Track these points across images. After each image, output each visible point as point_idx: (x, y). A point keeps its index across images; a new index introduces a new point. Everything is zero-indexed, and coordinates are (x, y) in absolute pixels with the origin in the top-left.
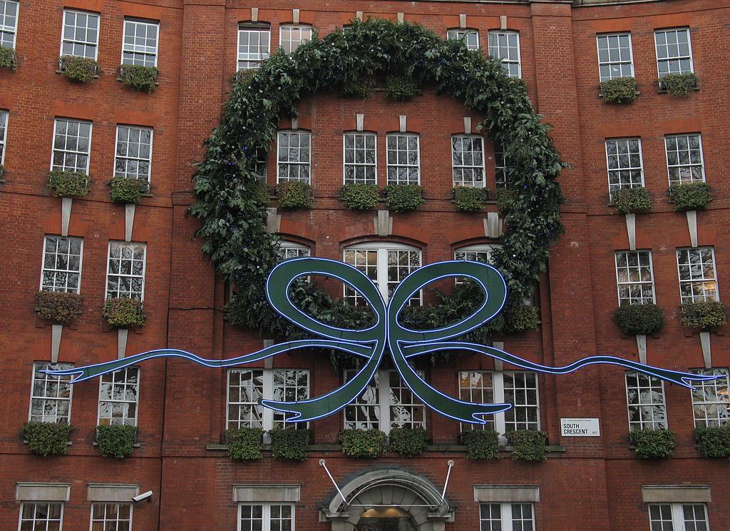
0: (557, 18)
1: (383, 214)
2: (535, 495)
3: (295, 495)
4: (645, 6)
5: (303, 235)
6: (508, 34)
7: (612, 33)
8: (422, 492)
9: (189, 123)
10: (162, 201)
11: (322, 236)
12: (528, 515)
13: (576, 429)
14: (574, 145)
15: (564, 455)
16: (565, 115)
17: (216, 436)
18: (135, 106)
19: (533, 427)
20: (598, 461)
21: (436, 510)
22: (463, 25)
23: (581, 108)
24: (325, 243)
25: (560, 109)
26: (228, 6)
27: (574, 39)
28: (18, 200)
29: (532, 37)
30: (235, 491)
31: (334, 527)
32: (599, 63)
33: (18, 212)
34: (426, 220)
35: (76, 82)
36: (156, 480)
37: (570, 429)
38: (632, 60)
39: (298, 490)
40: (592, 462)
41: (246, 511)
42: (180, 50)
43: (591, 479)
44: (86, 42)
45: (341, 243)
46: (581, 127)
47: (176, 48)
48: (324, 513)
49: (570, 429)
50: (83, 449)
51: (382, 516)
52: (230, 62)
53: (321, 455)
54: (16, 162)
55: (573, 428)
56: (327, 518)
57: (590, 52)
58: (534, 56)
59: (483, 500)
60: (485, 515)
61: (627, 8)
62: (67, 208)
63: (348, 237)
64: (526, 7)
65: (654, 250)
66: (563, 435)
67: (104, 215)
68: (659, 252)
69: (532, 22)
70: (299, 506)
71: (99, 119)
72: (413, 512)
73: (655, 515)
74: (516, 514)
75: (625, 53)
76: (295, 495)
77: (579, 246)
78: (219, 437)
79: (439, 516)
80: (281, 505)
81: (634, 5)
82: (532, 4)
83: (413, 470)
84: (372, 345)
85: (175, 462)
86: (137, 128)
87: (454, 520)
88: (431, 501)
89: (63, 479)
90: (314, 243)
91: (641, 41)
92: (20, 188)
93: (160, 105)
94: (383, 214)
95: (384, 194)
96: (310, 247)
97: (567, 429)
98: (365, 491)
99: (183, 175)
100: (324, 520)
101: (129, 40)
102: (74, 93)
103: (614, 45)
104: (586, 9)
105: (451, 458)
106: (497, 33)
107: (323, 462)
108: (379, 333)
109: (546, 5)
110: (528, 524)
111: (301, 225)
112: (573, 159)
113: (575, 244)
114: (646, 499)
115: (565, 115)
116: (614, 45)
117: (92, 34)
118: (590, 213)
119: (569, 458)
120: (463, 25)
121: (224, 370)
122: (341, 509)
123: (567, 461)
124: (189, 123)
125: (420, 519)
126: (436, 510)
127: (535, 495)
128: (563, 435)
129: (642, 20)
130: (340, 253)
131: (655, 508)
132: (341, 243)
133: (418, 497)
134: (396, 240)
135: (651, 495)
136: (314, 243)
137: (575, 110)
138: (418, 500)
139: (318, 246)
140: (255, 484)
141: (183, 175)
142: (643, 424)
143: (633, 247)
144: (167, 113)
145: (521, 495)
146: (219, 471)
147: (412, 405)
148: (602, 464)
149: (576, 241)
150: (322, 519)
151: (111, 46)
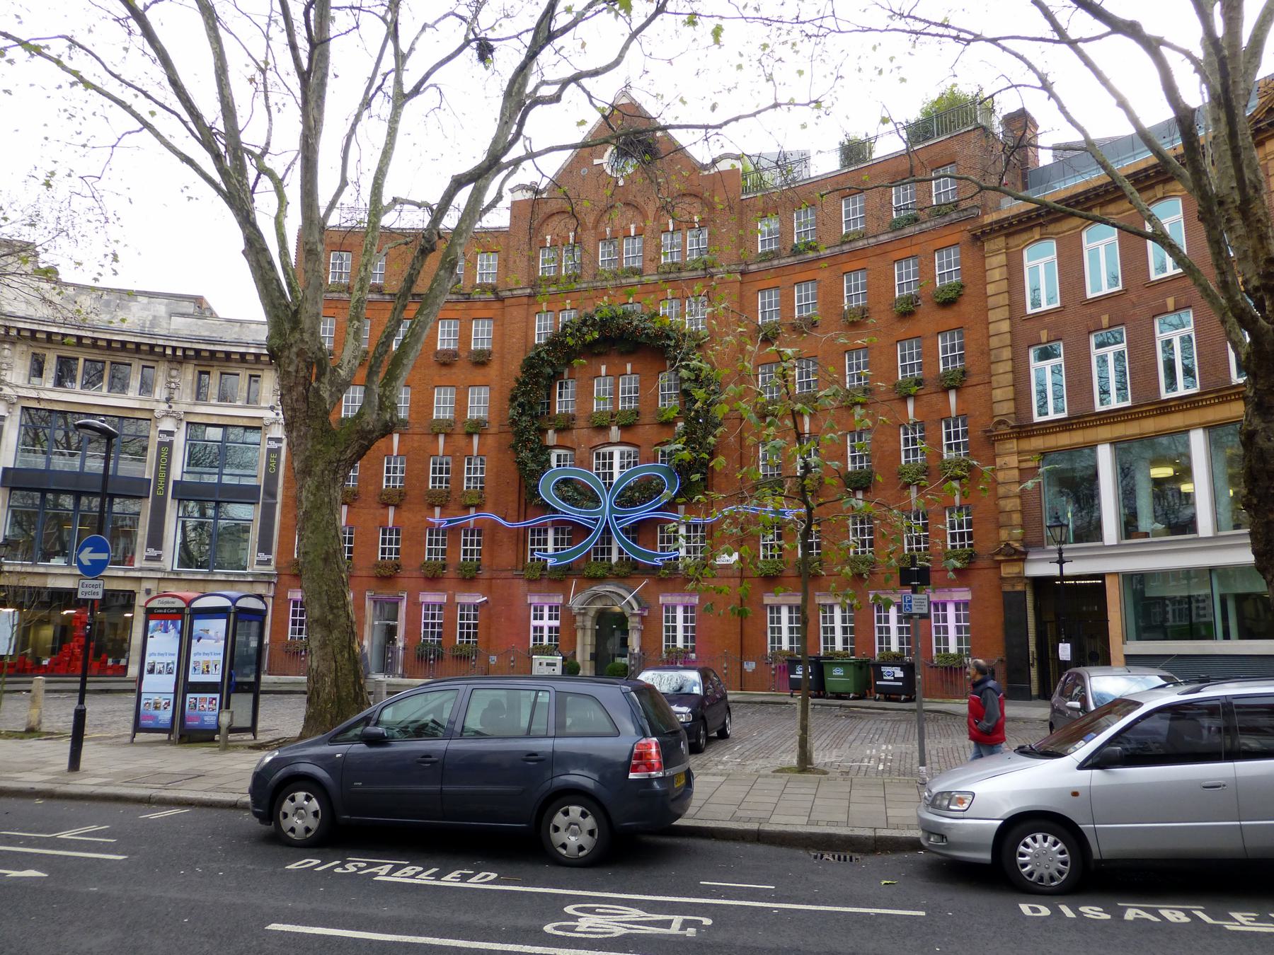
1: (614, 429)
5: (569, 445)
10: (493, 430)
11: (579, 445)
17: (520, 567)
18: (479, 374)
22: (670, 297)
28: (416, 437)
33: (416, 445)
34: (640, 430)
35: (444, 364)
36: (489, 591)
40: (732, 580)
42: (503, 335)
47: (500, 336)
50: (452, 575)
54: (414, 416)
62: (441, 439)
67: (460, 441)
73: (772, 612)
83: (1089, 209)
84: (597, 520)
89: (443, 591)
92: (417, 430)
93: (493, 371)
94: (614, 429)
95: (613, 416)
102: (444, 371)
108: (603, 512)
111: (569, 439)
114: (765, 602)
121: (526, 529)
127: (696, 600)
135: (769, 599)
140: (539, 592)
145: (687, 600)
146: (521, 586)
151: (464, 338)
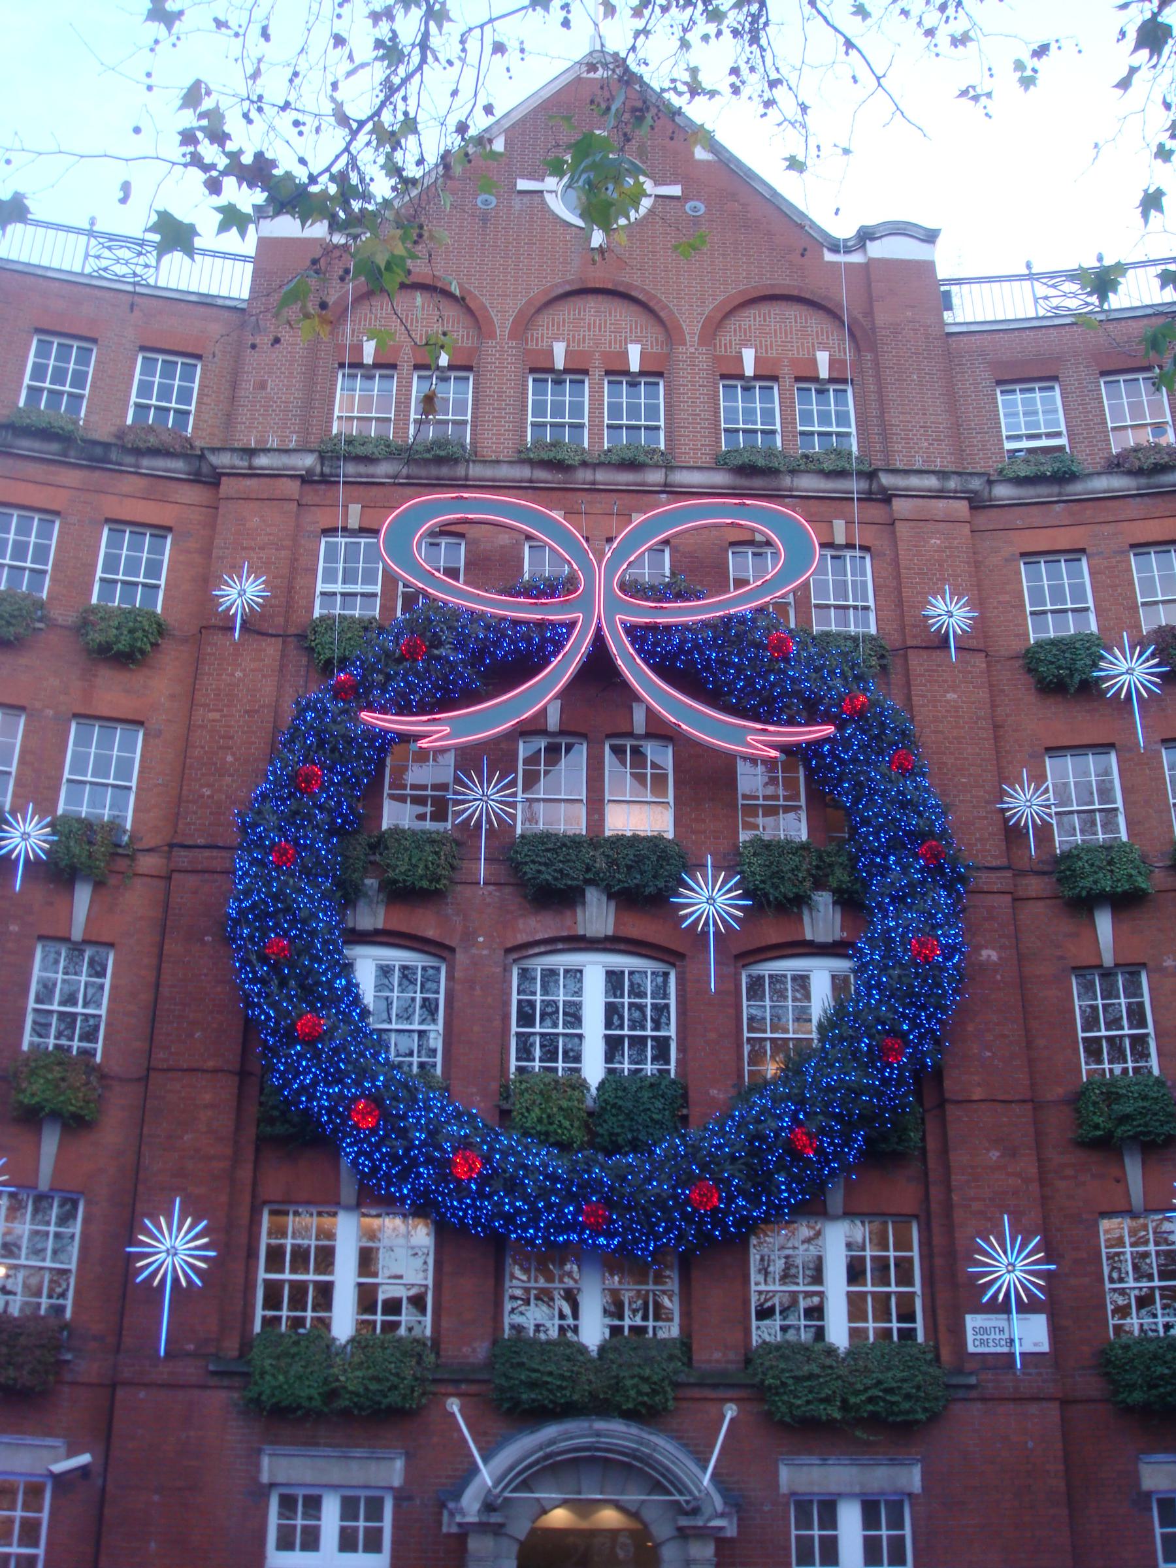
0: (944, 524)
2: (912, 1478)
3: (394, 1472)
4: (1109, 504)
6: (848, 554)
7: (1052, 554)
8: (666, 1472)
9: (212, 715)
12: (897, 1523)
13: (998, 1337)
14: (982, 760)
15: (974, 1394)
16: (963, 702)
19: (907, 1335)
20: (1044, 1404)
21: (695, 1512)
23: (993, 690)
24: (474, 951)
25: (955, 692)
26: (303, 502)
27: (977, 564)
29: (896, 562)
30: (265, 1461)
31: (474, 1544)
32: (1028, 609)
37: (985, 1337)
38: (1091, 604)
39: (399, 1464)
40: (1033, 1409)
41: (288, 1503)
43: (1030, 1445)
44: (1069, 606)
45: (508, 951)
46: (996, 727)
48: (452, 1515)
49: (985, 1337)
51: (584, 1525)
52: (303, 603)
53: (451, 1389)
55: (993, 1337)
56: (460, 1525)
57: (1008, 587)
58: (900, 592)
59: (802, 1489)
60: (804, 1521)
61: (1075, 507)
63: (522, 938)
64: (881, 505)
65: (1151, 964)
66: (971, 1349)
68: (1161, 970)
69: (894, 533)
70: (401, 1497)
71: (38, 705)
72: (649, 1515)
74: (870, 1518)
75: (1078, 592)
76: (394, 1472)
77: (1000, 958)
78: (237, 1346)
79: (700, 1523)
80: (363, 1494)
81: (1090, 504)
82: (224, 479)
85: (142, 1395)
86: (92, 722)
87: (735, 1534)
88: (682, 1489)
90: (452, 950)
91: (1107, 567)
96: (443, 959)
97: (979, 1337)
98: (544, 1468)
99: (195, 813)
100: (454, 1530)
101: (330, 577)
103: (1054, 575)
104: (998, 510)
105: (731, 1400)
106: (750, 551)
107: (454, 1405)
109: (920, 501)
110: (897, 1545)
112: (983, 786)
113: (989, 954)
115: (963, 702)
116: (1054, 575)
117: (1078, 592)
118: (1021, 894)
119: (984, 1400)
120: (840, 539)
122: (489, 1507)
123: (979, 1405)
124: (212, 715)
125: (662, 1529)
126: (695, 1512)
127: (912, 1478)
128: (971, 1349)
129: (1107, 529)
130: (505, 970)
131: (803, 1506)
132: (508, 951)
133: (659, 1482)
134: (622, 947)
136: (452, 950)
137: (983, 695)
138: (657, 1487)
139: (460, 957)
141: (195, 813)
142: (654, 1328)
143: (1108, 960)
144: (172, 697)
147: (893, 1288)
148: (1053, 1410)
149: (993, 948)
150: (449, 1525)
